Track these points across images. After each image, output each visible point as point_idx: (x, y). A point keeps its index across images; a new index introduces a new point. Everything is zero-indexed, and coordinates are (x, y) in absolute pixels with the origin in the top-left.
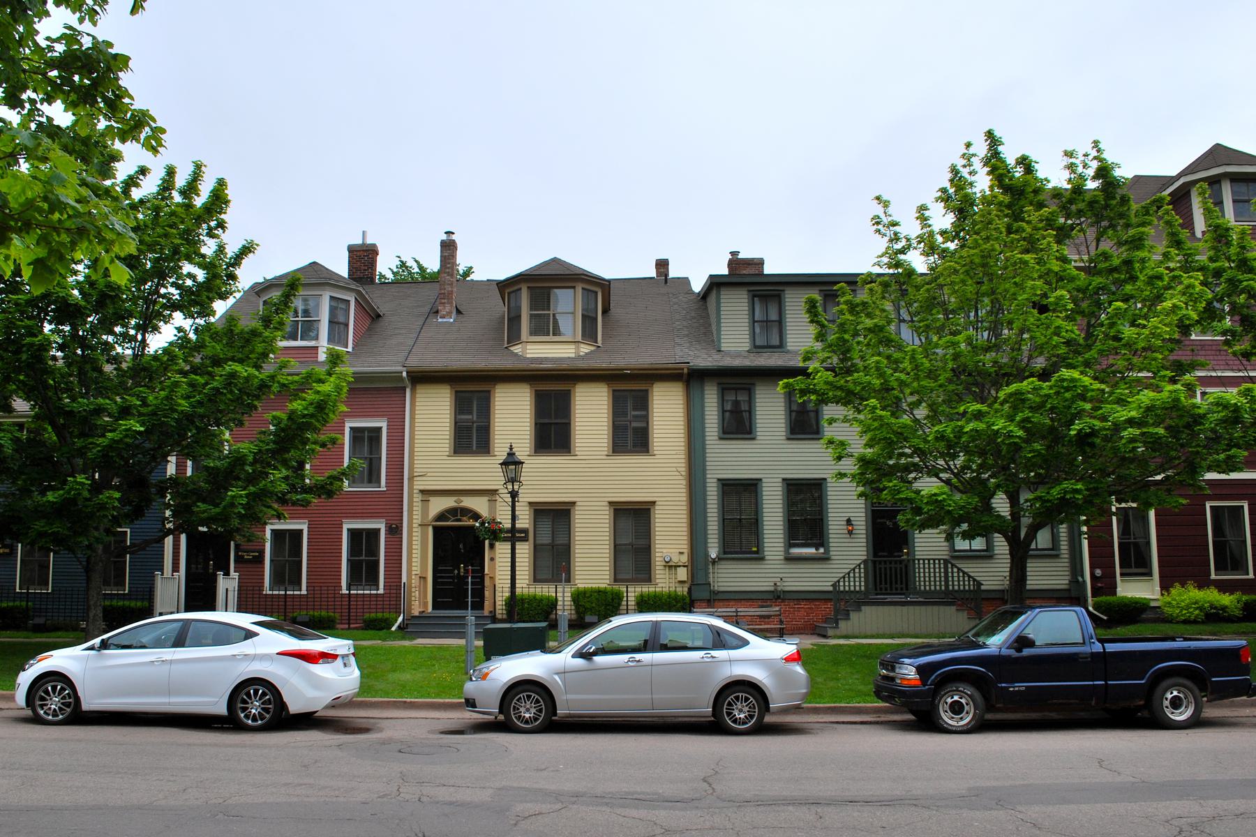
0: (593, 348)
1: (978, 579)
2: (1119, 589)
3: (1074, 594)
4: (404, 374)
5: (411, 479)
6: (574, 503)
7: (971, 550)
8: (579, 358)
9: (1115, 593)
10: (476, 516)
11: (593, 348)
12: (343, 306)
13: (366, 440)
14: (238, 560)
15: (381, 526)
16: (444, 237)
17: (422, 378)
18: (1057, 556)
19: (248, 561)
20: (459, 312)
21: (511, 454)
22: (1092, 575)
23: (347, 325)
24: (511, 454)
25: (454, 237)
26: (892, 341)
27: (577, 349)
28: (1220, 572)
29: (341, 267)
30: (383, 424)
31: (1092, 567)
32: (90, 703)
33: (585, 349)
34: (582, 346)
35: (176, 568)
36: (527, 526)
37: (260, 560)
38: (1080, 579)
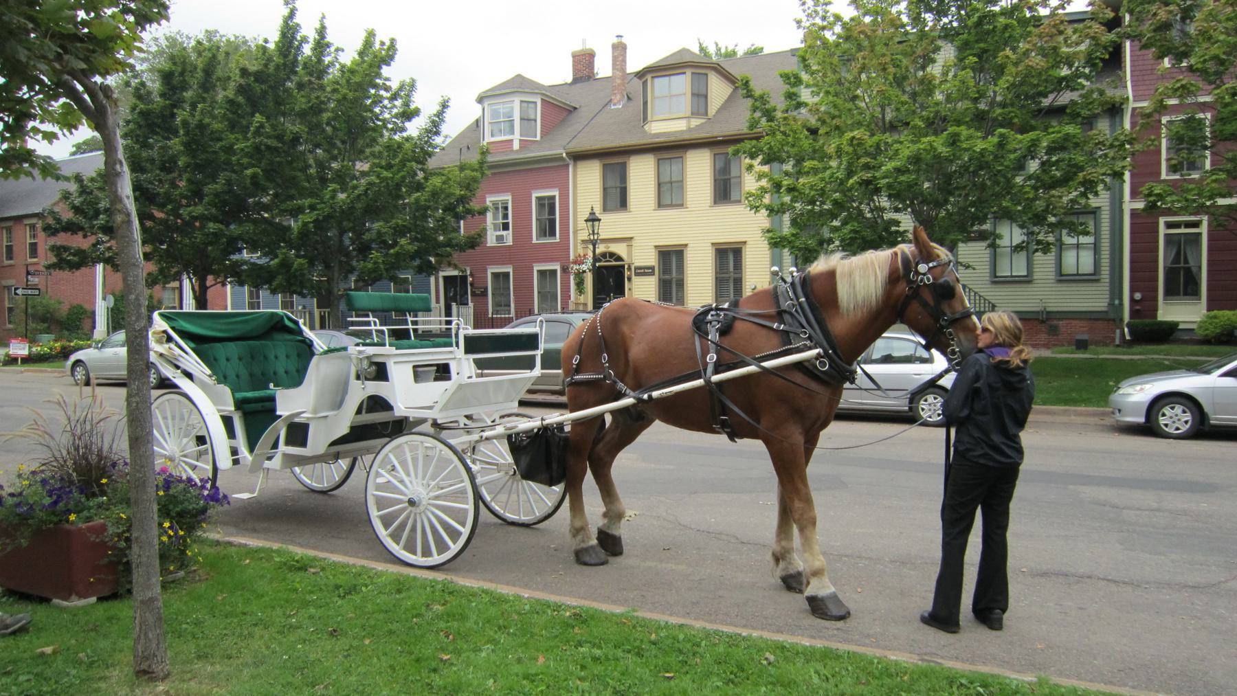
0: (703, 121)
1: (993, 301)
2: (1160, 312)
3: (1111, 316)
4: (564, 155)
5: (575, 232)
6: (686, 245)
7: (1012, 276)
8: (690, 130)
9: (1155, 316)
10: (619, 259)
11: (703, 121)
12: (532, 105)
13: (547, 205)
14: (473, 294)
15: (557, 267)
16: (616, 40)
17: (579, 157)
18: (1097, 281)
19: (478, 295)
20: (629, 98)
21: (593, 213)
22: (1132, 300)
23: (535, 120)
24: (593, 213)
25: (624, 40)
26: (398, 186)
27: (689, 122)
28: (1169, 298)
29: (413, 107)
30: (555, 193)
31: (1132, 291)
32: (1218, 418)
33: (695, 122)
34: (692, 120)
35: (438, 301)
36: (653, 264)
37: (485, 294)
38: (1117, 302)
